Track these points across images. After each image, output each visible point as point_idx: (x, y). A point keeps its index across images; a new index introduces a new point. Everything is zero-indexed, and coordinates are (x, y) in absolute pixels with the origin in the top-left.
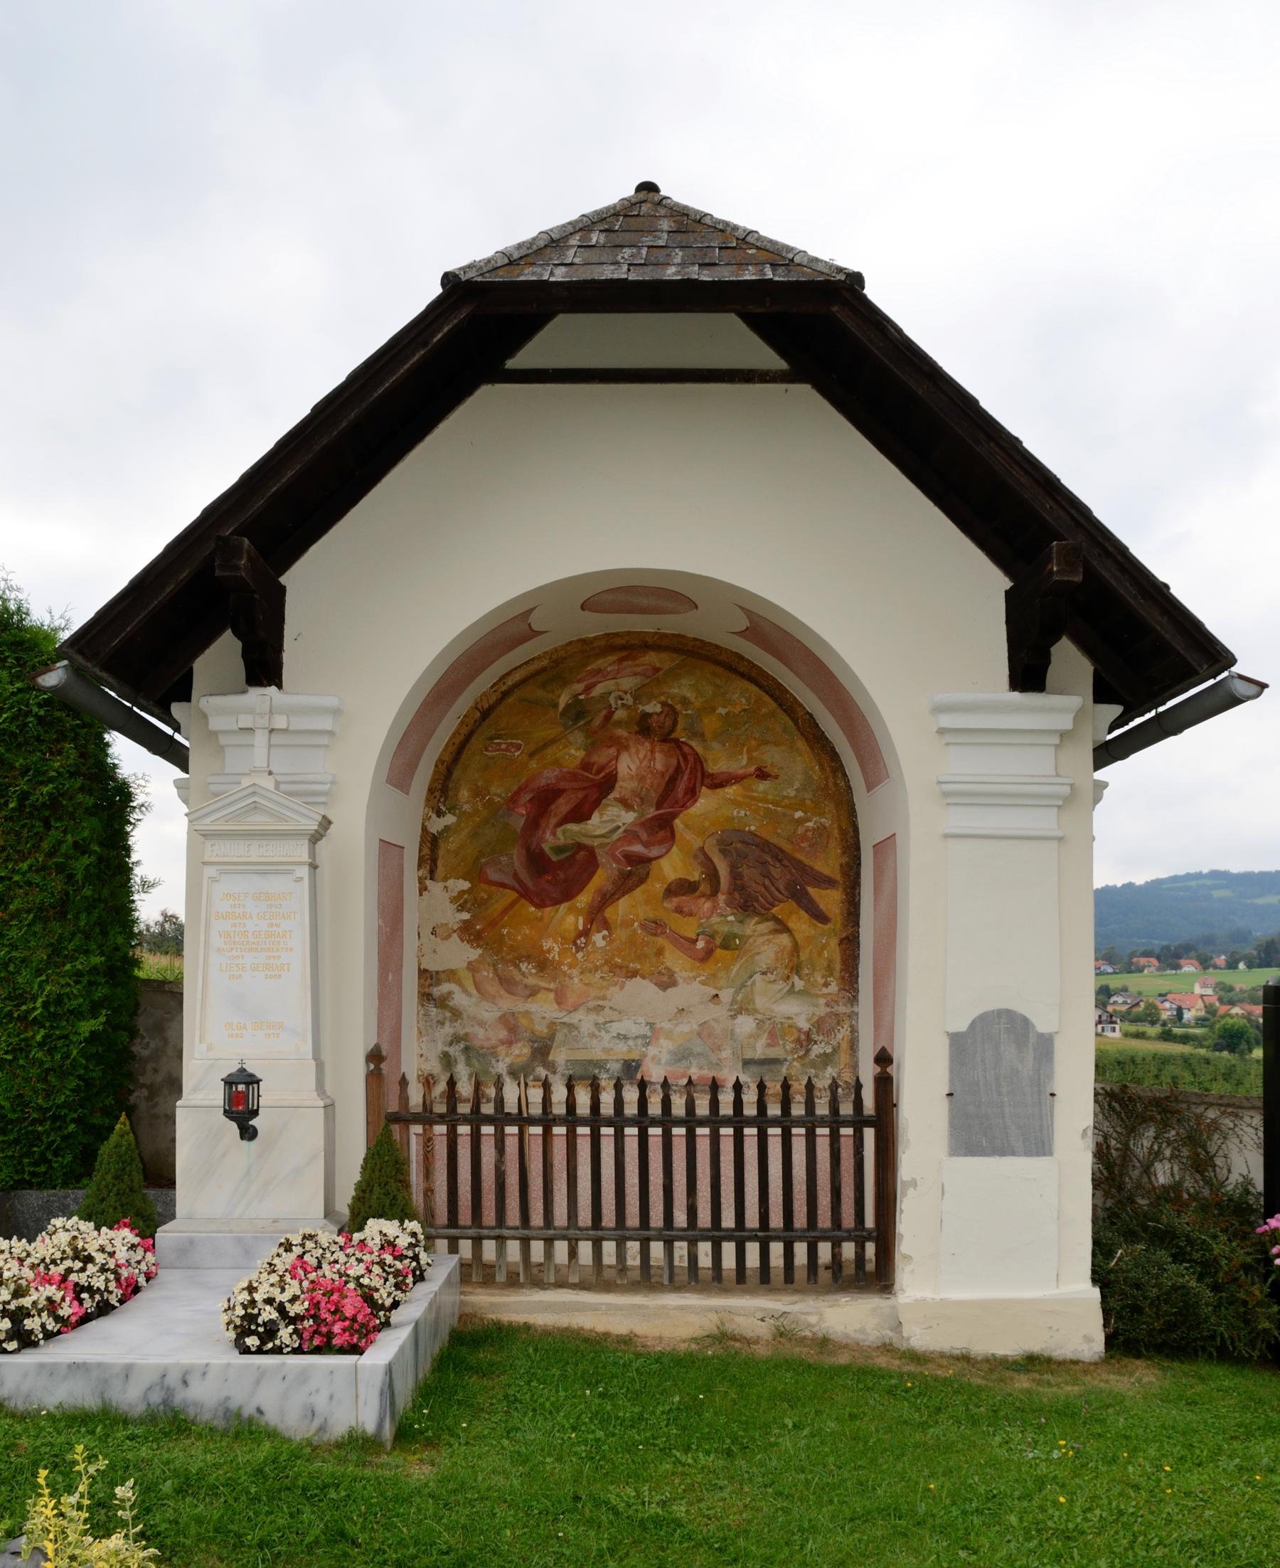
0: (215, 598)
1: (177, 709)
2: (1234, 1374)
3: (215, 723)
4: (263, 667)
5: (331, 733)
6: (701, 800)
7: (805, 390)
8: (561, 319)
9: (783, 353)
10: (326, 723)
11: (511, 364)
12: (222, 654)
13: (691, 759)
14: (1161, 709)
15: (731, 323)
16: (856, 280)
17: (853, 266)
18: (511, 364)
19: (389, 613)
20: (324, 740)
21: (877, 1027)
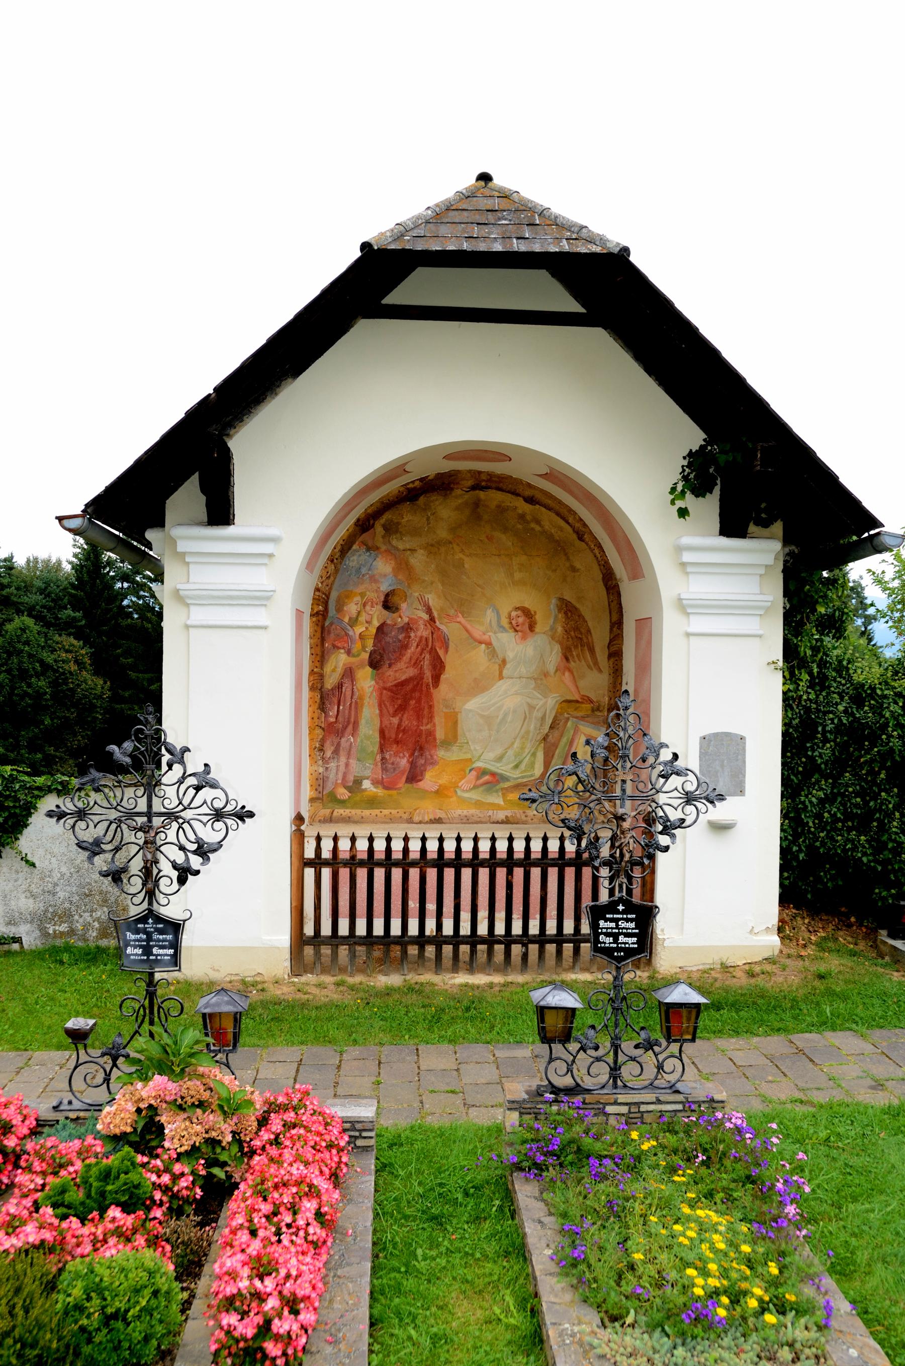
0: (190, 464)
1: (150, 535)
2: (820, 946)
3: (182, 546)
4: (220, 512)
5: (271, 556)
6: (860, 1098)
7: (598, 339)
8: (420, 270)
9: (577, 296)
10: (267, 548)
11: (389, 300)
12: (187, 498)
13: (768, 968)
14: (872, 532)
15: (542, 276)
16: (626, 250)
17: (625, 243)
18: (389, 300)
19: (305, 471)
20: (265, 561)
21: (571, 493)
